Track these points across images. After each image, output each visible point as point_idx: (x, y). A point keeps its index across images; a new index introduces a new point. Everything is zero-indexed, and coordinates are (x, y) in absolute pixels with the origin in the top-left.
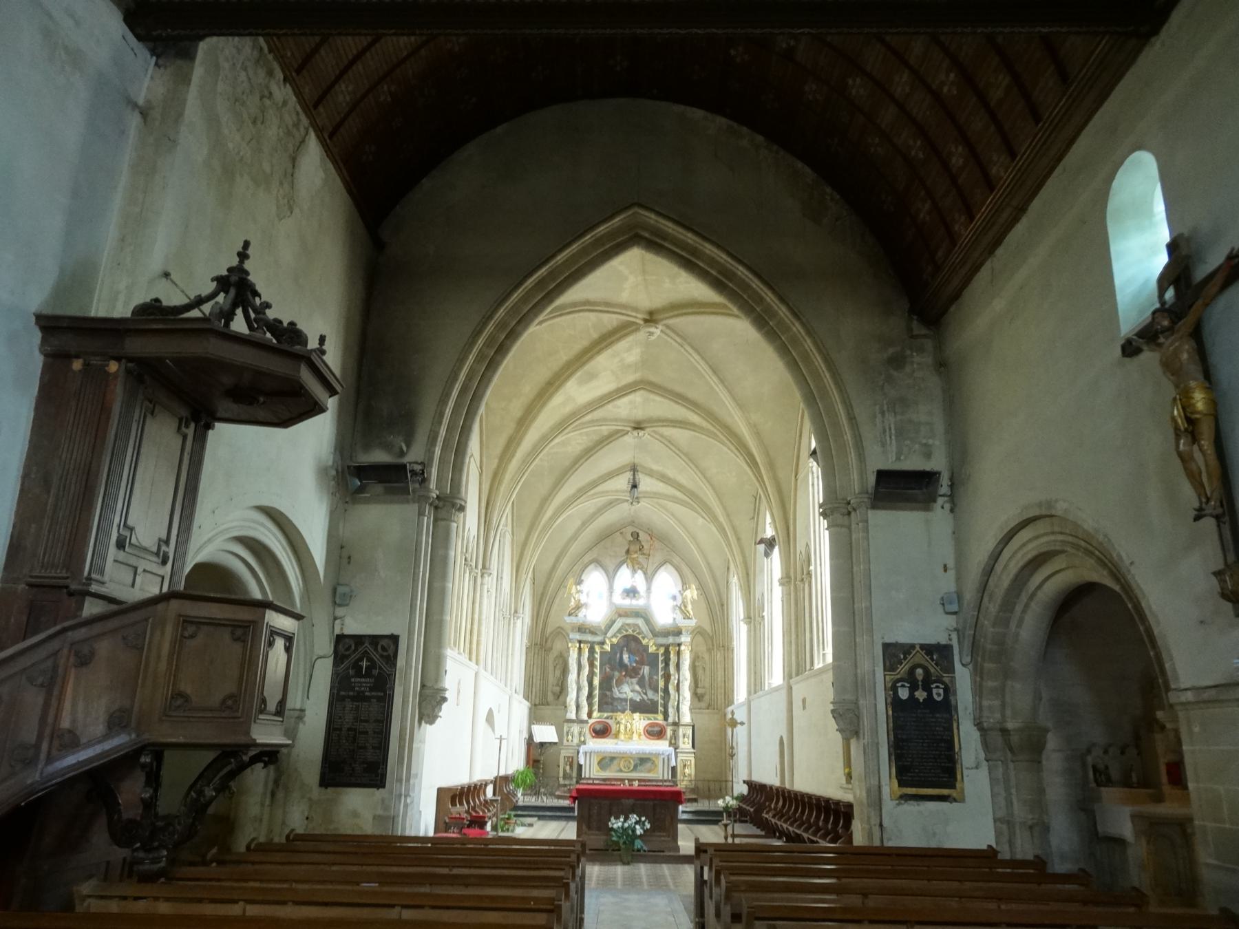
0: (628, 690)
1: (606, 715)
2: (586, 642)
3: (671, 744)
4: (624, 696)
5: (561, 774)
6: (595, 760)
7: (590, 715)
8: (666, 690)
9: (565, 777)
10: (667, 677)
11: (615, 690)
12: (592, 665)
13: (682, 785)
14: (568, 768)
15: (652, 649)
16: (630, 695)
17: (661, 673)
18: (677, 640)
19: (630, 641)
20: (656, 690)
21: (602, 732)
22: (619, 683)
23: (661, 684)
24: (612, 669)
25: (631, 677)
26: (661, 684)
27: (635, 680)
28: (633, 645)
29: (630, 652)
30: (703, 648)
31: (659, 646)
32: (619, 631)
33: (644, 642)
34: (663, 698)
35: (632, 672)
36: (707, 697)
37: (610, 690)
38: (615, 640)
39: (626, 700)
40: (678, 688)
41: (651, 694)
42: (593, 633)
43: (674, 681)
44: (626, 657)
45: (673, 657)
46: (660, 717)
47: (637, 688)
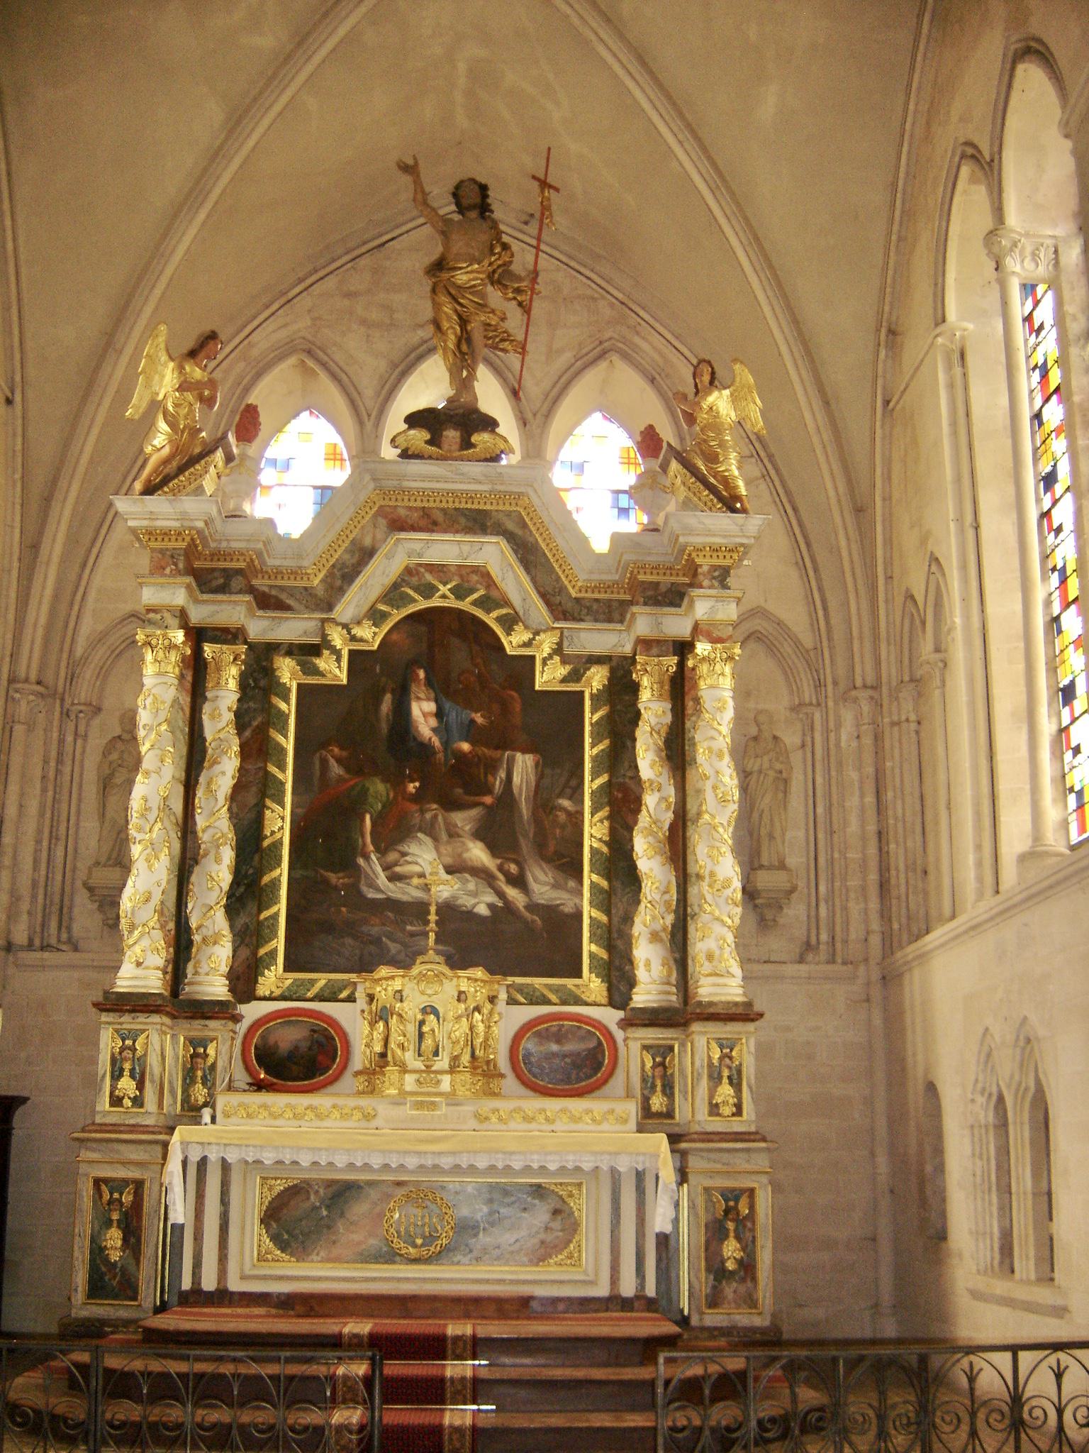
0: (433, 868)
1: (322, 980)
2: (228, 635)
3: (648, 1119)
4: (408, 893)
5: (81, 1278)
6: (249, 1203)
7: (244, 981)
8: (620, 864)
9: (97, 1289)
10: (623, 802)
11: (374, 866)
12: (257, 749)
13: (740, 1419)
14: (114, 1238)
15: (548, 677)
16: (445, 889)
17: (591, 784)
18: (676, 625)
19: (447, 642)
20: (568, 864)
21: (300, 1062)
22: (393, 834)
23: (594, 832)
24: (357, 767)
25: (451, 805)
26: (594, 832)
27: (464, 820)
28: (460, 656)
29: (442, 689)
30: (778, 703)
31: (580, 666)
32: (394, 595)
33: (513, 643)
34: (604, 900)
35: (455, 782)
36: (795, 912)
37: (346, 859)
38: (371, 636)
39: (419, 910)
40: (677, 845)
41: (543, 885)
42: (267, 602)
43: (655, 806)
44: (422, 711)
45: (653, 709)
46: (592, 984)
47: (478, 853)
